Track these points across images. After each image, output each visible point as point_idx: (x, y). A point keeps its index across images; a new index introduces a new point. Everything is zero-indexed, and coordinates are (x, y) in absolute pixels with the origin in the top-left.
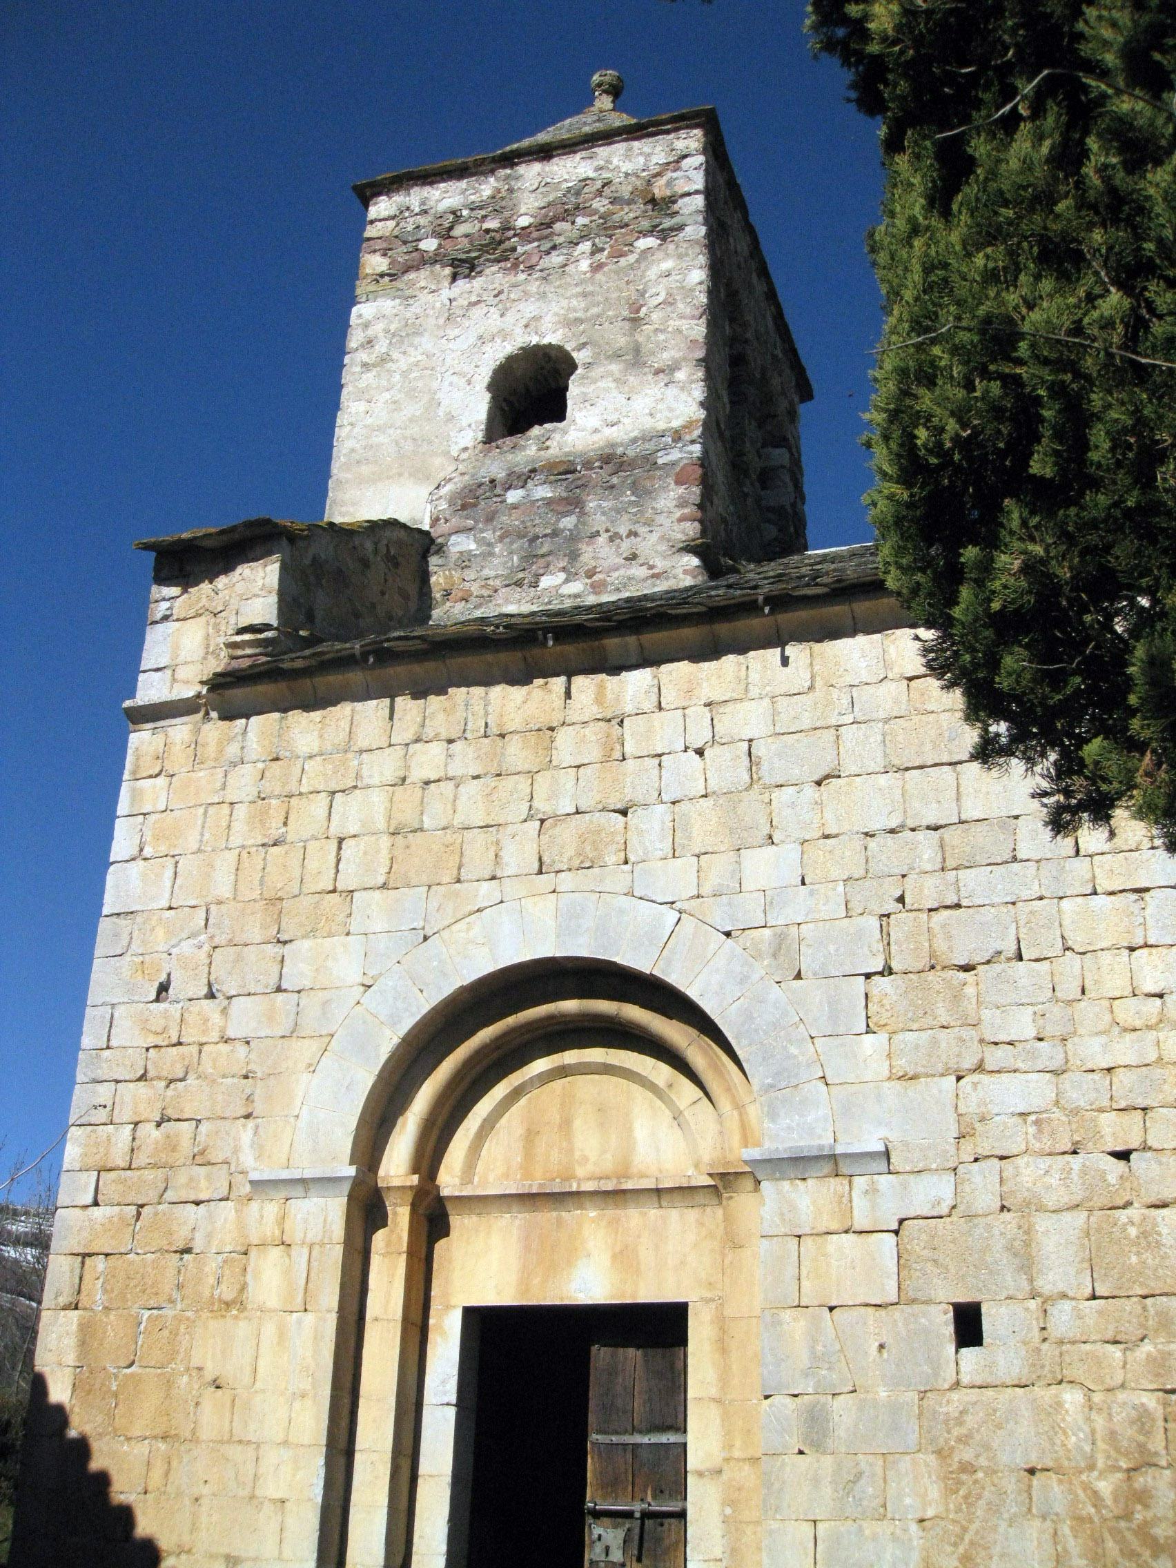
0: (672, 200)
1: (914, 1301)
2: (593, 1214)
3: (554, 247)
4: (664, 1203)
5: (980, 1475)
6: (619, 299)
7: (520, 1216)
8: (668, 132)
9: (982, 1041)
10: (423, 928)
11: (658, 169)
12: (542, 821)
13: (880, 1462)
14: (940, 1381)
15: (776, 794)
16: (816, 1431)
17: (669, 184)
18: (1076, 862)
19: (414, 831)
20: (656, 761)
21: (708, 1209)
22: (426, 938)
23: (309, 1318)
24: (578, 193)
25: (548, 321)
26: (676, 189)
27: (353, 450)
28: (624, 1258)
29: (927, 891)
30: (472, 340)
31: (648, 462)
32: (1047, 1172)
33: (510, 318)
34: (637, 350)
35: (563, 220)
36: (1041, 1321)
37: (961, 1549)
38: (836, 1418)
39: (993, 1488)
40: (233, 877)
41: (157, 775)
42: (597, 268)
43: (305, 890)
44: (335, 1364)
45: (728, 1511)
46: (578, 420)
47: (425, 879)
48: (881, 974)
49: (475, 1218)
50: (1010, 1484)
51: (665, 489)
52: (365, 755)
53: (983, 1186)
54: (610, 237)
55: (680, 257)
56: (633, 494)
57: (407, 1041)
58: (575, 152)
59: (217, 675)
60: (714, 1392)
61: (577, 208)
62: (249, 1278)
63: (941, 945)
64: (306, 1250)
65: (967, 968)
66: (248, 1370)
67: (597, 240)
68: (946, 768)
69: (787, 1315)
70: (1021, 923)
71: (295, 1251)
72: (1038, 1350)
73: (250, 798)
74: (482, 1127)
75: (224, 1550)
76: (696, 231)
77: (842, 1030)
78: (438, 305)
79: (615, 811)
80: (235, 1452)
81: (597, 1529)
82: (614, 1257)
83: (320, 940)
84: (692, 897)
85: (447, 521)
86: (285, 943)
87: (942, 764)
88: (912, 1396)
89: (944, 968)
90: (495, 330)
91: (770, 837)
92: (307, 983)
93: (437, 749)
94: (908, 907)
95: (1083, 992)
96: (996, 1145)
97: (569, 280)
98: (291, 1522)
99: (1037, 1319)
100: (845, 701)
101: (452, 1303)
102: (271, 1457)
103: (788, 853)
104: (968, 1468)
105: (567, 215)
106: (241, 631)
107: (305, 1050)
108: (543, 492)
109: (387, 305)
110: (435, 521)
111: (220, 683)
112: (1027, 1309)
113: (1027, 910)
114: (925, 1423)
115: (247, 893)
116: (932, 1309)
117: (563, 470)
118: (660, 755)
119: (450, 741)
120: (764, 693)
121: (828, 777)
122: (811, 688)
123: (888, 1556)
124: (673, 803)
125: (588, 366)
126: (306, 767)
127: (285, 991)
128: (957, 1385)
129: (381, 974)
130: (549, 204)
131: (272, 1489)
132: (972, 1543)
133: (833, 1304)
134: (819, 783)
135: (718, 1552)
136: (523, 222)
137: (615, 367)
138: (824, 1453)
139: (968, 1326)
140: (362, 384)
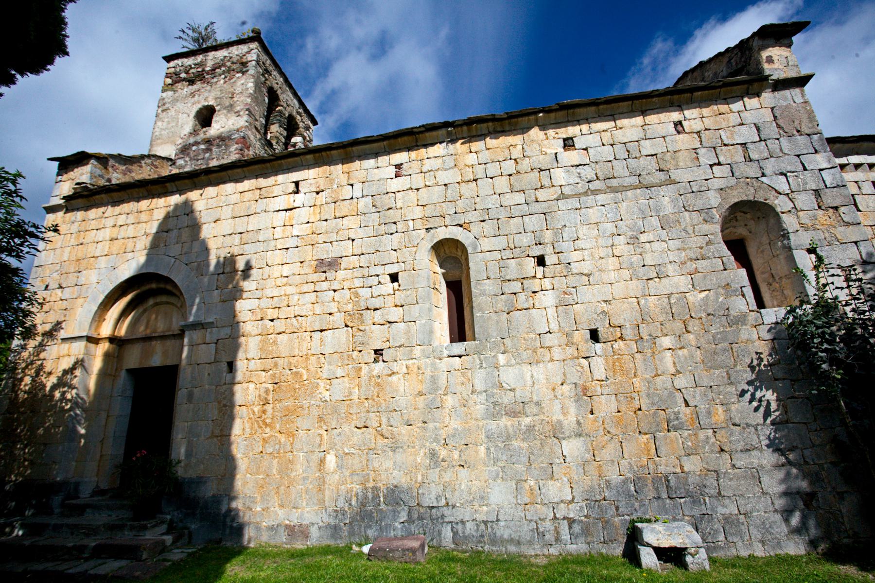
0: (247, 63)
25: (210, 99)
42: (225, 82)
57: (106, 297)
88: (214, 387)
93: (124, 216)
104: (225, 406)
105: (219, 67)
107: (80, 301)
108: (202, 147)
117: (208, 141)
136: (208, 69)
137: (225, 111)
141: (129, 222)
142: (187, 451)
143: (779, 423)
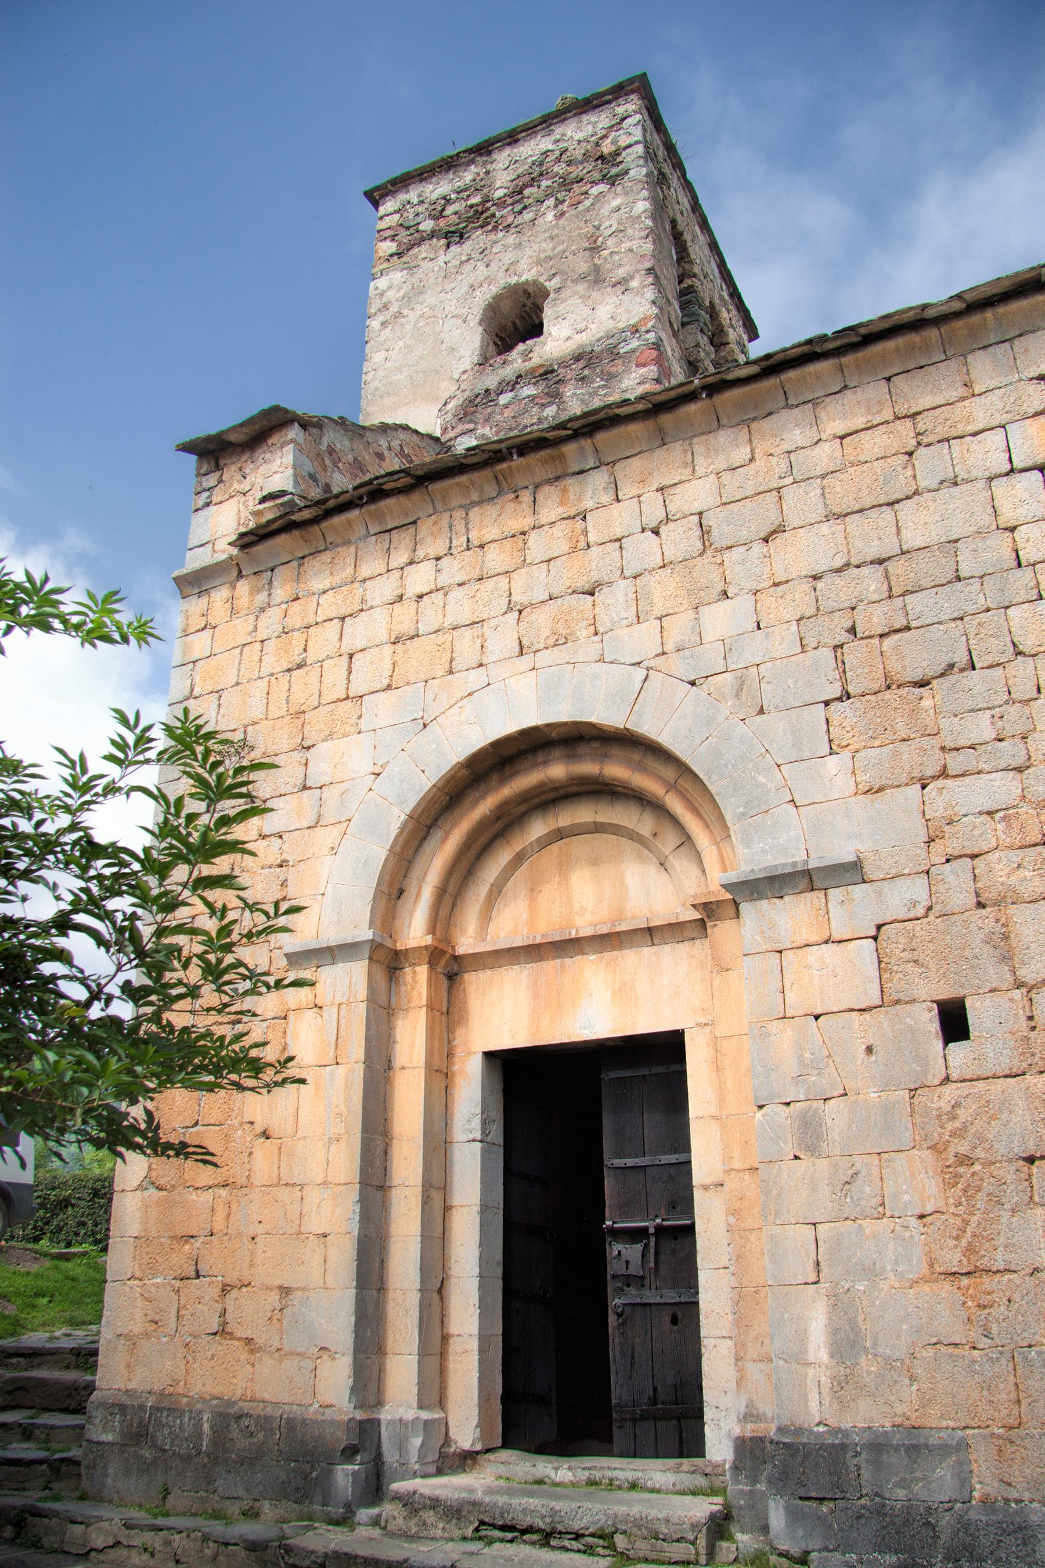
0: (617, 153)
1: (897, 1002)
2: (592, 957)
3: (525, 208)
4: (656, 941)
5: (977, 1167)
6: (579, 235)
7: (528, 966)
8: (609, 102)
9: (943, 748)
10: (422, 718)
11: (604, 132)
12: (520, 612)
13: (876, 1162)
14: (930, 1077)
15: (727, 555)
16: (810, 1136)
17: (613, 142)
18: (1019, 573)
19: (412, 638)
20: (618, 544)
21: (698, 942)
22: (425, 726)
23: (341, 1070)
24: (541, 164)
25: (523, 265)
26: (619, 144)
27: (377, 389)
28: (623, 993)
29: (874, 619)
30: (465, 289)
31: (612, 353)
32: (1019, 866)
33: (493, 267)
34: (597, 269)
35: (531, 186)
36: (1027, 1009)
37: (964, 1242)
38: (829, 1122)
39: (992, 1180)
40: (265, 701)
41: (203, 629)
43: (323, 702)
44: (364, 1108)
45: (732, 1220)
46: (553, 333)
47: (422, 677)
48: (840, 699)
49: (488, 972)
50: (1008, 1172)
51: (628, 371)
52: (368, 583)
53: (956, 886)
54: (569, 191)
55: (627, 194)
56: (602, 379)
58: (536, 132)
59: (242, 535)
60: (714, 1110)
61: (541, 175)
62: (288, 1039)
63: (894, 666)
64: (335, 1010)
65: (923, 684)
66: (291, 1120)
67: (559, 195)
68: (884, 508)
69: (774, 1027)
70: (971, 636)
71: (325, 1012)
72: (1027, 1038)
73: (276, 634)
74: (491, 891)
75: (278, 1282)
76: (638, 172)
77: (806, 755)
78: (436, 269)
79: (583, 593)
80: (283, 1194)
81: (616, 1248)
82: (614, 993)
83: (336, 741)
84: (657, 655)
85: (453, 428)
86: (308, 748)
87: (880, 505)
89: (899, 687)
90: (482, 278)
91: (725, 593)
92: (327, 779)
93: (428, 567)
94: (858, 636)
95: (1039, 691)
96: (966, 843)
97: (538, 229)
98: (332, 1253)
99: (1024, 1008)
100: (784, 466)
101: (473, 1050)
102: (314, 1195)
103: (743, 603)
104: (965, 1160)
105: (533, 182)
106: (263, 500)
107: (327, 836)
109: (397, 276)
110: (445, 430)
111: (251, 540)
112: (1011, 1000)
113: (975, 623)
114: (918, 1120)
115: (276, 711)
116: (915, 1007)
118: (619, 540)
119: (438, 559)
120: (709, 471)
121: (774, 532)
122: (752, 460)
123: (890, 1253)
124: (635, 578)
125: (558, 290)
126: (321, 601)
127: (310, 788)
128: (947, 1079)
129: (388, 762)
130: (519, 177)
131: (316, 1224)
132: (974, 1235)
133: (818, 1011)
134: (766, 540)
135: (725, 1261)
136: (500, 193)
137: (580, 288)
138: (819, 1156)
139: (954, 1023)
140: (382, 338)
141: (444, 580)
142: (834, 1331)
143: (236, 1063)
